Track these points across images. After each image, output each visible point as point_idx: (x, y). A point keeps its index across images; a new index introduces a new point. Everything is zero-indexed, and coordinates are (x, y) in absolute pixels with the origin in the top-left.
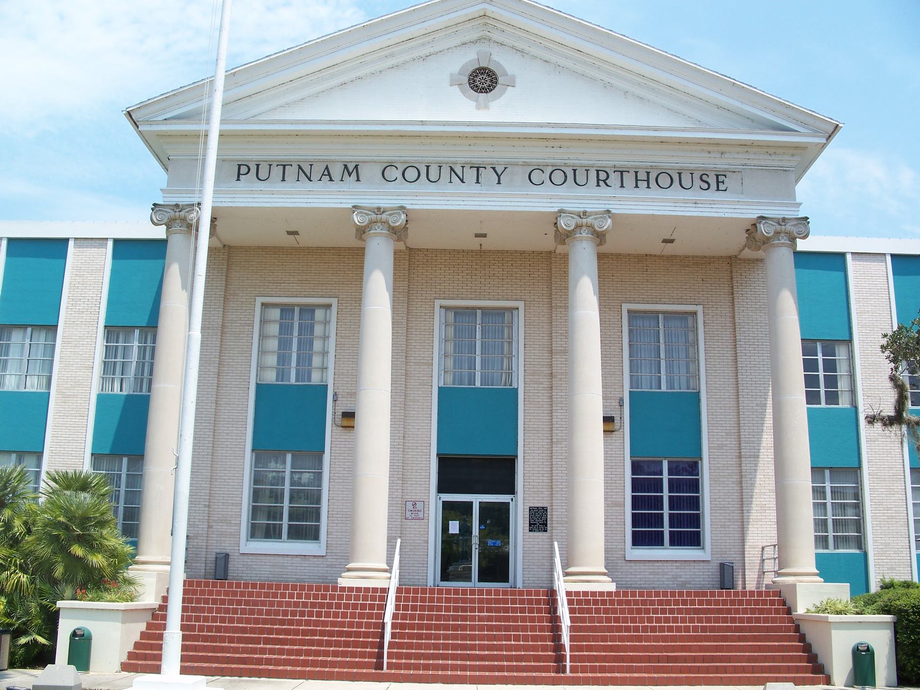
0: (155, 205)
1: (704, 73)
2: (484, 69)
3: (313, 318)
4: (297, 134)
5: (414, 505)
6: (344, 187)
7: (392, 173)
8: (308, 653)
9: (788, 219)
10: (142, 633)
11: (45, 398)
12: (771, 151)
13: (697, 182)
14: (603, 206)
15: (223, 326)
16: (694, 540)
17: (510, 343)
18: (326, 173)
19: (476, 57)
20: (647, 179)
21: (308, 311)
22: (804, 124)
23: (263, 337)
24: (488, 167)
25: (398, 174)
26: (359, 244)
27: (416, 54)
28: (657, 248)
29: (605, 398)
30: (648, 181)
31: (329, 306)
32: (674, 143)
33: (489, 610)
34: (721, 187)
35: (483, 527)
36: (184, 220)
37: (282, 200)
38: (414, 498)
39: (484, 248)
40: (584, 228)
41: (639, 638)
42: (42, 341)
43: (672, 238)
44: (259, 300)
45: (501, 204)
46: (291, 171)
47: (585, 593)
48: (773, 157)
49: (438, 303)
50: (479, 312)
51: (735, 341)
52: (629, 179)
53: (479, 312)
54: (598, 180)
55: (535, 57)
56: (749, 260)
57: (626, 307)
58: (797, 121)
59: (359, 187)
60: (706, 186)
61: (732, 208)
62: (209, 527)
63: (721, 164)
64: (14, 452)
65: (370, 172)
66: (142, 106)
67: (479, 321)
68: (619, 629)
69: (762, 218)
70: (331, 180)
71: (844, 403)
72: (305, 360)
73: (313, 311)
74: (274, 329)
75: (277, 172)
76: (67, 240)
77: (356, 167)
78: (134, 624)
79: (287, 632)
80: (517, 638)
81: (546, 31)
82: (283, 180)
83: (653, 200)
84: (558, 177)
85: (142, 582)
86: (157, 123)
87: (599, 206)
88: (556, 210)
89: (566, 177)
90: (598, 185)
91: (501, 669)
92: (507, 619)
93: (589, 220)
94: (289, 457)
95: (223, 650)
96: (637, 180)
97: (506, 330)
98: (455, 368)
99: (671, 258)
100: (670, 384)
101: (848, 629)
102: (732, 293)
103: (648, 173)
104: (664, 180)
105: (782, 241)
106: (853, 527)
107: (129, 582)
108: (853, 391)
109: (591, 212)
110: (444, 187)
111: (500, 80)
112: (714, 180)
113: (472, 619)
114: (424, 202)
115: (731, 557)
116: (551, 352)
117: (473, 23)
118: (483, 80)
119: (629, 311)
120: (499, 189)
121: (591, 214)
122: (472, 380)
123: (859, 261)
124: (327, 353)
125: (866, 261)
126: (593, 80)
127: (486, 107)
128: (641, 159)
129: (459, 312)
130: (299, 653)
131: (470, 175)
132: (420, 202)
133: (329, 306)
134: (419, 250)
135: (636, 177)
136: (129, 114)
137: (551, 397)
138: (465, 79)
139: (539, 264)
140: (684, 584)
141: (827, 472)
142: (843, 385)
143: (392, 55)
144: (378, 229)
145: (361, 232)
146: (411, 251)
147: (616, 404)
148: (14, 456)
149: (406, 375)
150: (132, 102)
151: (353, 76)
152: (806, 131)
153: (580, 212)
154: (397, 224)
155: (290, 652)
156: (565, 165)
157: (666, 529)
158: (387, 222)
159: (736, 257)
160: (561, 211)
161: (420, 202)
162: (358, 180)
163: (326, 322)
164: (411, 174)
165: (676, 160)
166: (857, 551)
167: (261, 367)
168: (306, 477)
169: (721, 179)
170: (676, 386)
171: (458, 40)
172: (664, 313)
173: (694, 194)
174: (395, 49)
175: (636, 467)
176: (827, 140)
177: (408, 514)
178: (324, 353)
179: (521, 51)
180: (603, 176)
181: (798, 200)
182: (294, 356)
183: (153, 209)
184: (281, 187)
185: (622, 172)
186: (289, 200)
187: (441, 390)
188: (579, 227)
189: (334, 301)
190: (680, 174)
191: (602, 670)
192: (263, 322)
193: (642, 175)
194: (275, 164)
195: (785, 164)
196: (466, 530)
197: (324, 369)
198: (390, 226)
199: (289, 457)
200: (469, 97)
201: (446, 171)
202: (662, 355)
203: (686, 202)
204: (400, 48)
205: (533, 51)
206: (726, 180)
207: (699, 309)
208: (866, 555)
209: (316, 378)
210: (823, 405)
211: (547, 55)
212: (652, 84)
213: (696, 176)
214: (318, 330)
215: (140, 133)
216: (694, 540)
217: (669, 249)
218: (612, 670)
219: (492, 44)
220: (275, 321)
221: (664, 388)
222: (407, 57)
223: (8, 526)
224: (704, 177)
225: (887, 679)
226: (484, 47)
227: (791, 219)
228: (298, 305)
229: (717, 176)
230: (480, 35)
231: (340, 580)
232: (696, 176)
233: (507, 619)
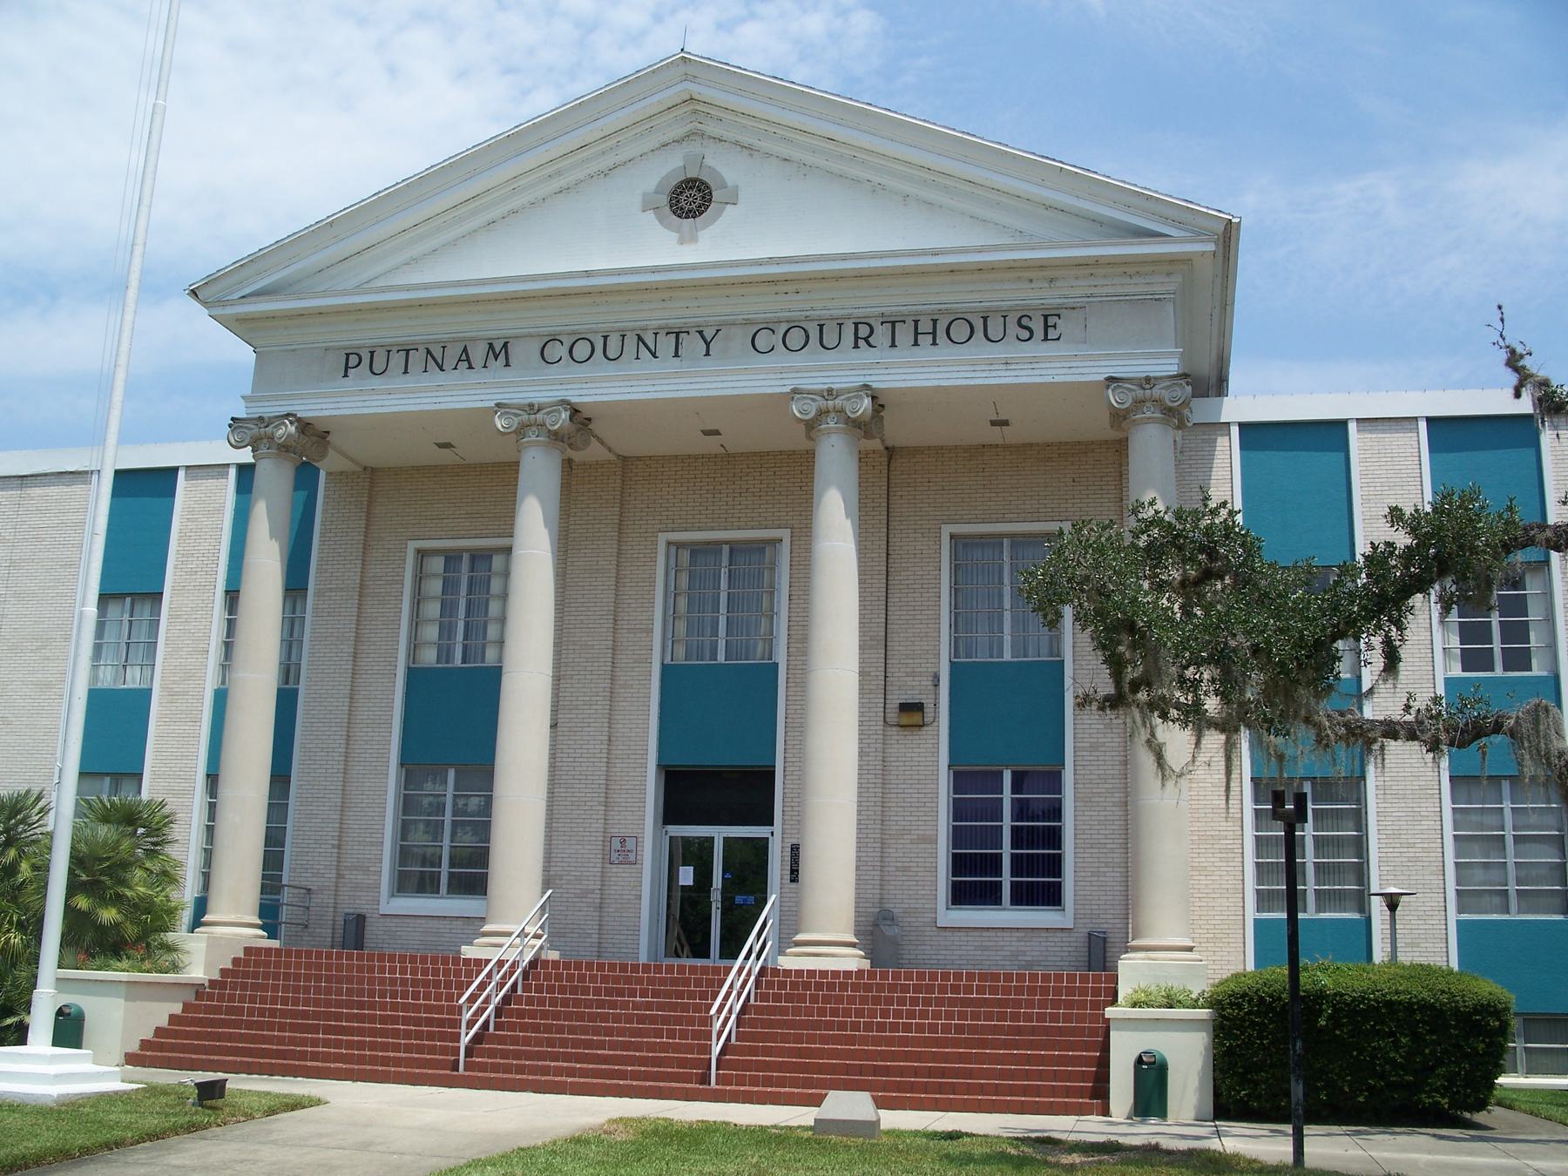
2: (694, 180)
4: (422, 305)
5: (623, 842)
8: (373, 1046)
10: (172, 1017)
11: (146, 694)
12: (1130, 270)
13: (1013, 329)
15: (362, 586)
16: (1050, 896)
20: (931, 329)
22: (1177, 223)
24: (693, 331)
25: (562, 351)
26: (807, 445)
27: (594, 167)
30: (934, 333)
32: (972, 271)
33: (656, 994)
34: (1052, 334)
35: (728, 876)
38: (624, 832)
41: (851, 1040)
42: (146, 616)
44: (412, 546)
45: (708, 386)
46: (417, 358)
47: (811, 973)
48: (1136, 280)
49: (663, 538)
54: (857, 338)
55: (769, 155)
57: (947, 530)
58: (1165, 219)
59: (508, 375)
60: (1026, 334)
62: (339, 876)
63: (1048, 297)
64: (108, 774)
65: (525, 352)
68: (829, 1025)
70: (470, 367)
71: (1538, 670)
75: (397, 360)
76: (176, 469)
78: (155, 1004)
79: (596, 1031)
80: (671, 1034)
81: (774, 114)
82: (406, 372)
83: (938, 364)
85: (186, 947)
86: (231, 303)
87: (855, 380)
88: (787, 389)
89: (808, 337)
90: (856, 346)
91: (622, 1075)
92: (673, 1007)
94: (451, 774)
95: (265, 1040)
96: (916, 334)
101: (1136, 1029)
103: (935, 321)
104: (960, 331)
105: (1148, 414)
106: (1352, 877)
107: (169, 948)
108: (1552, 647)
110: (396, 381)
112: (1041, 325)
113: (625, 1005)
115: (1108, 922)
119: (952, 536)
121: (839, 393)
123: (1370, 432)
125: (1383, 431)
127: (693, 239)
128: (923, 300)
129: (699, 551)
130: (361, 1046)
132: (592, 392)
134: (639, 458)
138: (664, 200)
139: (763, 471)
140: (1029, 965)
141: (1506, 785)
142: (1535, 640)
143: (559, 173)
145: (1119, 417)
146: (891, 452)
147: (927, 682)
148: (108, 779)
150: (197, 275)
152: (1183, 234)
155: (350, 1045)
157: (1006, 879)
161: (592, 392)
164: (796, 338)
165: (977, 297)
166: (1356, 916)
167: (414, 646)
168: (474, 803)
169: (1051, 321)
172: (1012, 536)
173: (1011, 349)
175: (960, 780)
177: (614, 856)
179: (749, 148)
184: (895, 356)
187: (665, 668)
190: (985, 319)
191: (768, 1082)
192: (420, 578)
193: (925, 326)
194: (394, 349)
195: (1157, 289)
196: (703, 876)
199: (451, 774)
200: (668, 227)
201: (631, 341)
205: (765, 145)
206: (1059, 322)
208: (1369, 920)
210: (1499, 671)
211: (785, 151)
216: (1050, 896)
218: (781, 1082)
223: (12, 869)
224: (1025, 321)
225: (1199, 1110)
226: (694, 148)
227: (1161, 378)
228: (467, 550)
229: (1046, 317)
230: (687, 129)
231: (464, 948)
233: (673, 1007)
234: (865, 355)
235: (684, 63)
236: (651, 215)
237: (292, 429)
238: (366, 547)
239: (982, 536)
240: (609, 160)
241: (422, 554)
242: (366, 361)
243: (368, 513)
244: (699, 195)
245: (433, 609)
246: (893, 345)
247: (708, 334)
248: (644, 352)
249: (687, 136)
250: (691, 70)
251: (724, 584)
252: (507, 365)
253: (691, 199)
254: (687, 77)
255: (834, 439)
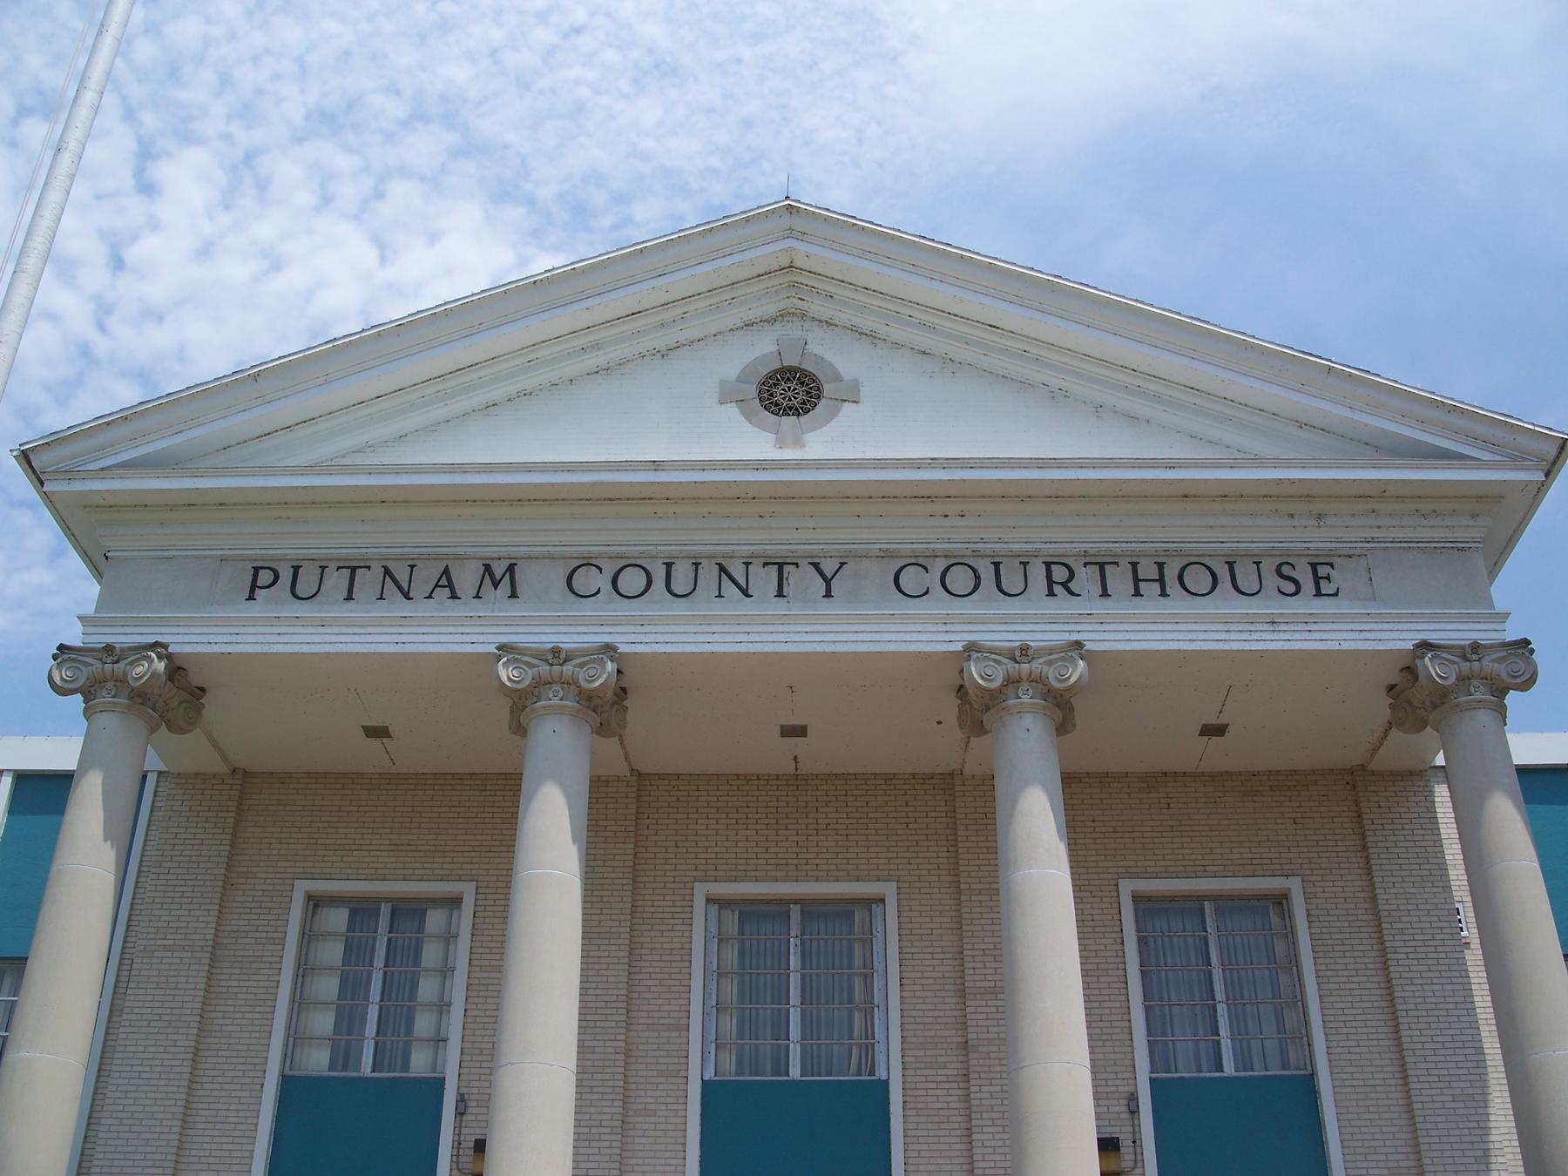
0: (62, 648)
1: (1264, 351)
3: (421, 929)
6: (478, 609)
7: (589, 580)
9: (1485, 647)
13: (1271, 581)
14: (1066, 637)
15: (216, 945)
17: (868, 979)
18: (444, 581)
19: (775, 348)
20: (1157, 576)
21: (409, 912)
22: (1492, 445)
23: (304, 969)
24: (804, 563)
25: (602, 581)
27: (648, 343)
28: (1189, 752)
29: (1098, 1097)
30: (1161, 580)
31: (455, 902)
34: (1326, 588)
36: (122, 680)
37: (343, 638)
39: (806, 767)
40: (1025, 686)
43: (1222, 721)
44: (302, 887)
49: (701, 890)
50: (795, 911)
51: (1383, 952)
52: (1119, 579)
53: (795, 911)
54: (1051, 582)
55: (899, 346)
56: (1392, 773)
58: (1475, 439)
59: (515, 610)
60: (1291, 588)
61: (1361, 629)
63: (1319, 539)
65: (540, 580)
66: (56, 441)
67: (795, 929)
69: (1425, 646)
70: (454, 596)
72: (397, 1021)
73: (424, 912)
74: (333, 952)
75: (337, 581)
77: (511, 569)
82: (349, 598)
83: (1177, 619)
84: (960, 579)
86: (85, 476)
87: (1057, 636)
88: (959, 647)
89: (977, 577)
93: (1036, 666)
96: (1136, 580)
97: (857, 947)
98: (741, 1036)
99: (1220, 778)
100: (1244, 1060)
102: (1365, 848)
103: (1160, 565)
105: (1478, 696)
109: (1039, 649)
111: (828, 389)
112: (1311, 575)
114: (660, 638)
116: (962, 993)
117: (772, 282)
118: (790, 392)
119: (1137, 899)
120: (828, 608)
121: (1041, 652)
122: (781, 1065)
124: (449, 1005)
126: (1026, 385)
129: (754, 913)
131: (764, 580)
132: (652, 638)
133: (455, 902)
134: (660, 776)
135: (1135, 573)
136: (25, 457)
137: (967, 1097)
138: (752, 390)
143: (597, 346)
144: (553, 698)
147: (1119, 1108)
149: (627, 1053)
151: (512, 388)
153: (1013, 649)
154: (597, 684)
156: (976, 554)
158: (573, 682)
159: (1363, 767)
160: (971, 648)
162: (513, 595)
163: (449, 938)
165: (1216, 534)
167: (295, 1039)
169: (1322, 571)
170: (1257, 1062)
171: (735, 317)
172: (1216, 898)
174: (602, 335)
176: (1547, 475)
178: (442, 1006)
179: (872, 337)
180: (1060, 574)
181: (1499, 608)
182: (373, 1013)
183: (55, 657)
185: (1102, 566)
186: (357, 639)
187: (706, 1086)
188: (1011, 682)
189: (467, 890)
192: (308, 937)
193: (1147, 570)
197: (439, 1041)
198: (581, 691)
200: (760, 425)
201: (709, 574)
202: (1219, 994)
203: (1251, 620)
204: (612, 332)
205: (896, 332)
206: (1333, 573)
207: (1295, 885)
209: (420, 1062)
212: (1152, 387)
213: (1268, 567)
214: (431, 954)
215: (46, 496)
217: (1218, 754)
219: (807, 325)
220: (335, 935)
221: (1229, 1069)
222: (629, 350)
224: (1286, 570)
226: (794, 330)
229: (1314, 566)
230: (782, 305)
232: (1268, 567)
234: (1064, 605)
235: (791, 216)
236: (732, 410)
237: (160, 666)
238: (227, 885)
239: (1172, 898)
240: (663, 340)
241: (315, 902)
242: (285, 579)
243: (234, 835)
244: (801, 397)
245: (327, 987)
246: (1105, 594)
247: (829, 567)
248: (730, 589)
249: (783, 316)
250: (799, 223)
251: (794, 962)
252: (514, 595)
253: (790, 392)
254: (791, 233)
255: (1029, 721)
